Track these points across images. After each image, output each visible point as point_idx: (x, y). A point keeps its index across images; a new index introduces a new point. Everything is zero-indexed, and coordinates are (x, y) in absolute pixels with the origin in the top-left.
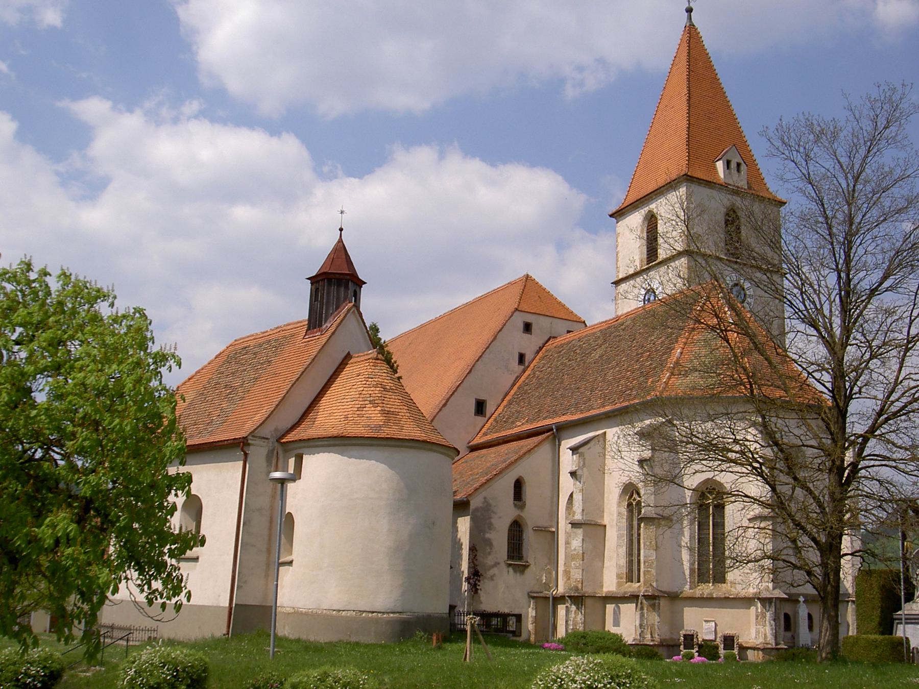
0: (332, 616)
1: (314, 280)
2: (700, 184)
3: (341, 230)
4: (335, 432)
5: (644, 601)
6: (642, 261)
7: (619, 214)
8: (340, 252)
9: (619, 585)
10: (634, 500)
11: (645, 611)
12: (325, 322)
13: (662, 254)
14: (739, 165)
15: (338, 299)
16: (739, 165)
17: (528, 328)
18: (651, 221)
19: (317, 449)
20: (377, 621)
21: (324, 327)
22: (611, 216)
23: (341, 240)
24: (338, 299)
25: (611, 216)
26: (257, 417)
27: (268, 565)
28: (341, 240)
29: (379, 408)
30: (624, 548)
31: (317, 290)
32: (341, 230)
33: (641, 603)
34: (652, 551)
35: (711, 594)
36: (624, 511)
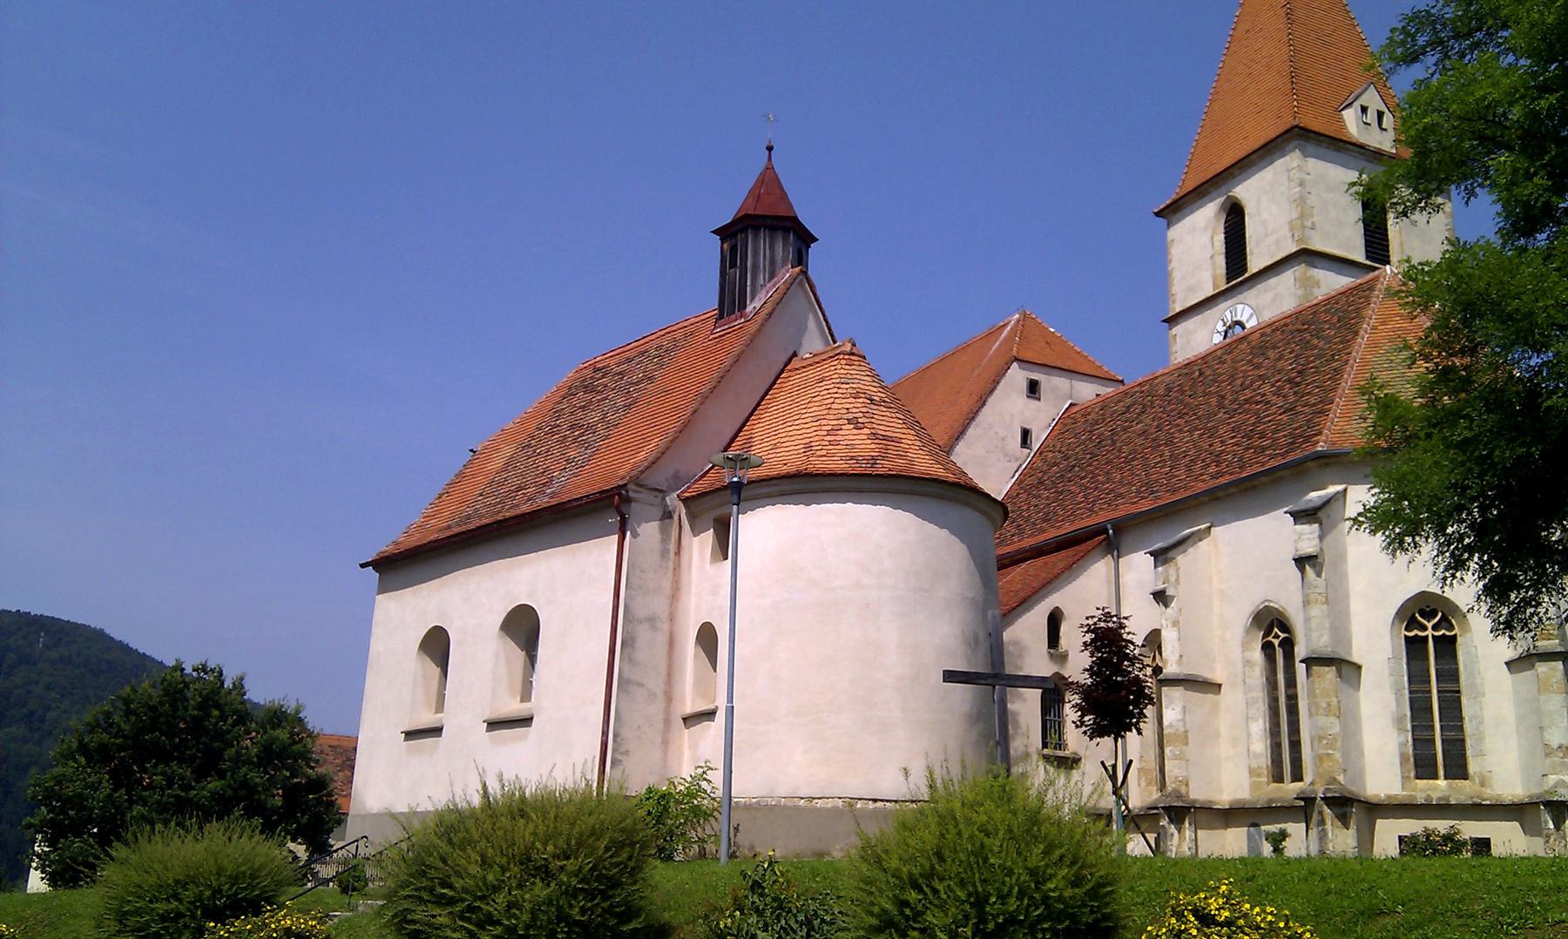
0: (796, 808)
1: (724, 233)
2: (1319, 144)
3: (770, 149)
4: (792, 469)
5: (1327, 811)
6: (1215, 278)
7: (1173, 211)
8: (769, 182)
9: (1254, 786)
10: (1277, 636)
11: (1328, 826)
12: (752, 299)
13: (1255, 263)
14: (1380, 115)
15: (773, 262)
16: (1380, 115)
17: (1033, 388)
18: (1235, 217)
19: (755, 502)
20: (885, 814)
21: (749, 309)
22: (1157, 214)
23: (769, 168)
24: (773, 262)
25: (1157, 214)
26: (642, 456)
27: (667, 722)
28: (769, 168)
29: (866, 431)
30: (1261, 722)
31: (733, 249)
32: (770, 149)
33: (1321, 813)
34: (1332, 719)
35: (1447, 798)
36: (1257, 655)
